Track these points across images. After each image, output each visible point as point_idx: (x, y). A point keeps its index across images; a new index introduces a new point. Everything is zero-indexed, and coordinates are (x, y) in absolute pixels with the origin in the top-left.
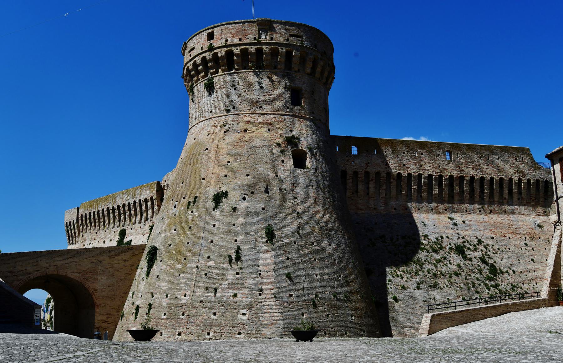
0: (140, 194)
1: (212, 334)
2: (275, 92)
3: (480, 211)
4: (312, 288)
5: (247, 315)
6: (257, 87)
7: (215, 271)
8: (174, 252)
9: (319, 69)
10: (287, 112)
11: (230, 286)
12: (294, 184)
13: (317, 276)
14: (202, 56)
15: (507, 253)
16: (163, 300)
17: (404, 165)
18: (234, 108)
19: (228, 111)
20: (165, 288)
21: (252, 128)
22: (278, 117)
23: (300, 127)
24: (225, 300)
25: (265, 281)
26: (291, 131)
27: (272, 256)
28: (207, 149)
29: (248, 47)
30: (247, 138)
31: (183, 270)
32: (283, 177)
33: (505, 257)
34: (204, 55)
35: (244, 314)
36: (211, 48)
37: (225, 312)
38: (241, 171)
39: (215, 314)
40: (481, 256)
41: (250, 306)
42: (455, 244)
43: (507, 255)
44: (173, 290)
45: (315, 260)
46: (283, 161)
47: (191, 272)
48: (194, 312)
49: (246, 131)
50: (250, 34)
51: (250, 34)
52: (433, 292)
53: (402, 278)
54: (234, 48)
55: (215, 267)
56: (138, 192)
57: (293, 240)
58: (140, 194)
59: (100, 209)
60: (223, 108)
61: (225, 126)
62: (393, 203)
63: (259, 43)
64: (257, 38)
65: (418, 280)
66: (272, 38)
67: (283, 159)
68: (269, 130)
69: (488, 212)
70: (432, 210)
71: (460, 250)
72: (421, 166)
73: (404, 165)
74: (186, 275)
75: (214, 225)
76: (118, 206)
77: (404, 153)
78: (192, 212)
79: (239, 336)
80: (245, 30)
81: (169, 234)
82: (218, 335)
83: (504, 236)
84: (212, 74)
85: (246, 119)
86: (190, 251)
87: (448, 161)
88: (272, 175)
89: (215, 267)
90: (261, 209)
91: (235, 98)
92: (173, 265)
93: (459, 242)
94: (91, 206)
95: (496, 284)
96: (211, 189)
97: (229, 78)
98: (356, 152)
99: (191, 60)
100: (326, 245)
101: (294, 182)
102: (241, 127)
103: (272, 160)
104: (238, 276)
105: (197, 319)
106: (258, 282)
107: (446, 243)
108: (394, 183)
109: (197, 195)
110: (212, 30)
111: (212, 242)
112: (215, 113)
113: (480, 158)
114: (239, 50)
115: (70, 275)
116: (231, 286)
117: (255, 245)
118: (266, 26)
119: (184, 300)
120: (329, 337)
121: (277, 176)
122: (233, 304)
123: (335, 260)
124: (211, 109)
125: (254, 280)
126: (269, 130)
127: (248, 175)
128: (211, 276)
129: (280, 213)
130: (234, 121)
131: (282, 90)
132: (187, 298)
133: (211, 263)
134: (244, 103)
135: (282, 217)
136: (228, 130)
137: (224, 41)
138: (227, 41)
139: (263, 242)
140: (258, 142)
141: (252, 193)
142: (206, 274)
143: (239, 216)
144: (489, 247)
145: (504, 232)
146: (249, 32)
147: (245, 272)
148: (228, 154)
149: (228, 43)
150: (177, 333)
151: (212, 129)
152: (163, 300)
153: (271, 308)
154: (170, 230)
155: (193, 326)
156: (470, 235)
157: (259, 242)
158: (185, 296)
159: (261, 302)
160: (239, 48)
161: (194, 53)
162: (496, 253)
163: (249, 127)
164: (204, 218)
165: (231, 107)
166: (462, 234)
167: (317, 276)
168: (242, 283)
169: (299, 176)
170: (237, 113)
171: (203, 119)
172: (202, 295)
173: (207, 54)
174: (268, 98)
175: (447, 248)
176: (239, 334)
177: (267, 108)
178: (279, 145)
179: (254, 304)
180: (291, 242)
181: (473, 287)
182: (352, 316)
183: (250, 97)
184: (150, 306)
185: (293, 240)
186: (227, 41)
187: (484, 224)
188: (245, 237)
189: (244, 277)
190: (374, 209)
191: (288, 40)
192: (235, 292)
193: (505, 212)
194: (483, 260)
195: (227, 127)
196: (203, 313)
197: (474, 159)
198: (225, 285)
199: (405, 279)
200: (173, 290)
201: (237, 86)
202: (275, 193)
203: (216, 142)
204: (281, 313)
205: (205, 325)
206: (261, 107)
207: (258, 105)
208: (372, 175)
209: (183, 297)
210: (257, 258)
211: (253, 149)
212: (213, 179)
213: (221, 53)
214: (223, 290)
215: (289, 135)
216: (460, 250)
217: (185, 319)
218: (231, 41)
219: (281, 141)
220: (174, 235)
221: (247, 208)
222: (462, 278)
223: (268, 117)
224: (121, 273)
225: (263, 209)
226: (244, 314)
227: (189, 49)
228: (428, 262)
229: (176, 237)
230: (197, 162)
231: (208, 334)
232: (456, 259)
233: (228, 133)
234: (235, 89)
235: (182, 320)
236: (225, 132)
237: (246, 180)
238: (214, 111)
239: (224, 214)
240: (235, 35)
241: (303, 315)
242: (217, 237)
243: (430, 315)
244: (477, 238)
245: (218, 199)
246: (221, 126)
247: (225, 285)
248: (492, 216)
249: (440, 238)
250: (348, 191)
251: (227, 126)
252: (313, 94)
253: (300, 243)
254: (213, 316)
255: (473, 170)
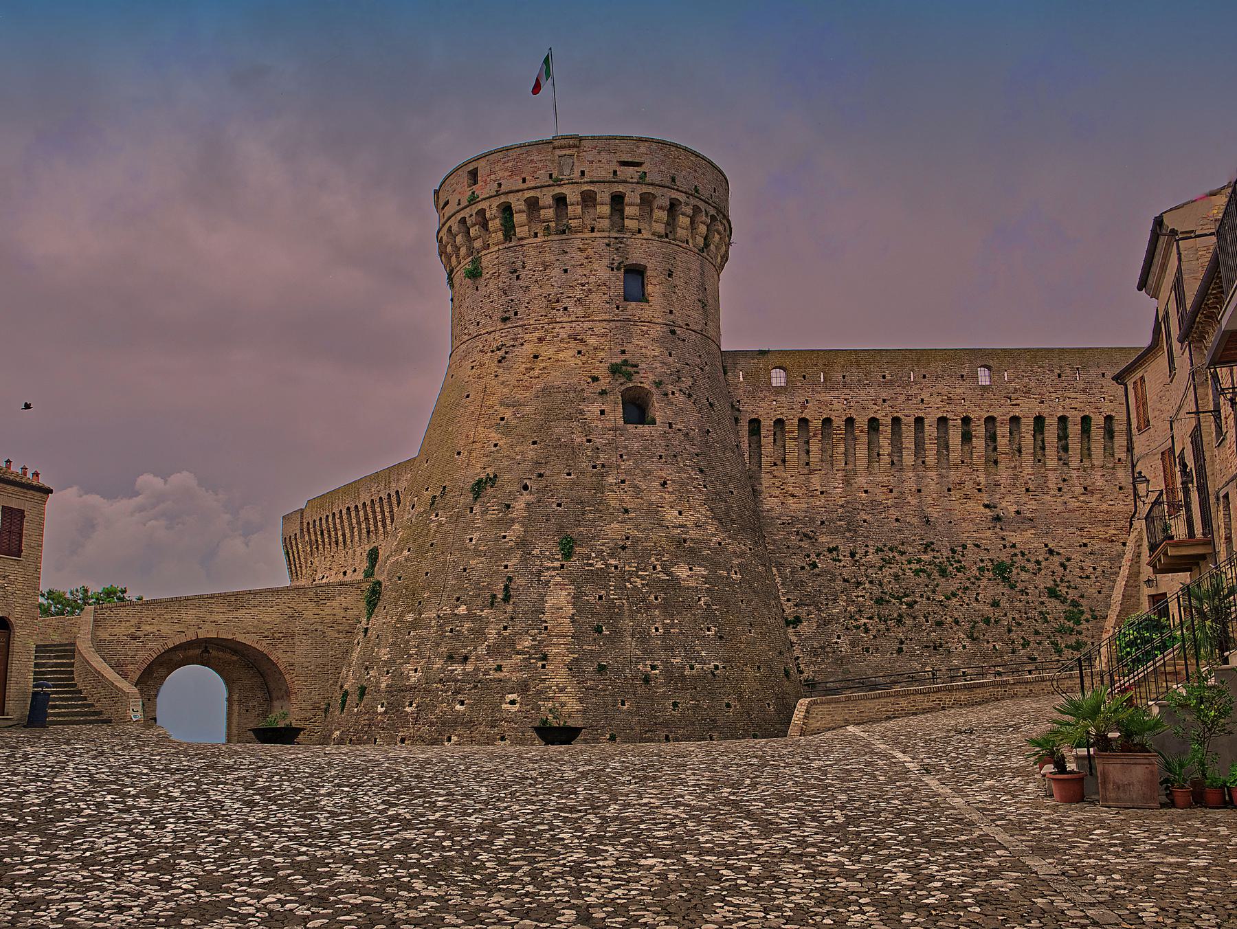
1: (454, 738)
4: (645, 651)
6: (556, 272)
10: (617, 315)
11: (493, 651)
12: (621, 456)
17: (884, 401)
18: (516, 314)
23: (641, 343)
24: (481, 676)
27: (569, 594)
31: (414, 625)
35: (513, 702)
36: (473, 200)
37: (479, 700)
38: (522, 435)
39: (462, 703)
40: (1050, 584)
41: (523, 687)
42: (992, 561)
45: (656, 599)
46: (602, 412)
47: (428, 626)
49: (536, 357)
59: (336, 511)
62: (861, 480)
67: (603, 407)
71: (1002, 571)
72: (922, 400)
75: (471, 540)
81: (400, 558)
85: (537, 334)
87: (984, 388)
93: (1004, 556)
95: (1077, 642)
98: (783, 380)
103: (582, 412)
104: (506, 633)
108: (863, 439)
109: (447, 483)
111: (465, 570)
122: (494, 685)
126: (579, 352)
127: (534, 443)
129: (590, 512)
131: (604, 274)
133: (462, 610)
135: (594, 521)
136: (504, 358)
139: (554, 569)
140: (556, 379)
141: (541, 475)
143: (513, 521)
144: (1073, 566)
146: (539, 165)
148: (502, 404)
153: (562, 690)
157: (548, 569)
159: (545, 680)
161: (449, 210)
162: (1088, 577)
164: (453, 526)
167: (657, 629)
171: (467, 337)
172: (443, 669)
176: (503, 739)
180: (607, 565)
181: (1024, 646)
185: (612, 561)
188: (524, 560)
192: (499, 662)
194: (1052, 593)
198: (482, 649)
202: (582, 473)
204: (581, 701)
205: (443, 724)
206: (566, 309)
208: (816, 424)
210: (542, 598)
211: (547, 391)
212: (474, 454)
214: (478, 658)
216: (1002, 571)
217: (413, 713)
219: (602, 372)
224: (339, 632)
226: (513, 702)
227: (441, 204)
228: (928, 599)
229: (409, 564)
232: (990, 589)
233: (504, 364)
234: (518, 277)
235: (407, 714)
236: (500, 361)
237: (531, 452)
238: (483, 322)
239: (488, 517)
240: (514, 172)
241: (623, 704)
242: (473, 562)
244: (1046, 545)
245: (479, 488)
251: (504, 349)
252: (670, 275)
253: (627, 568)
254: (458, 707)
255: (1042, 402)
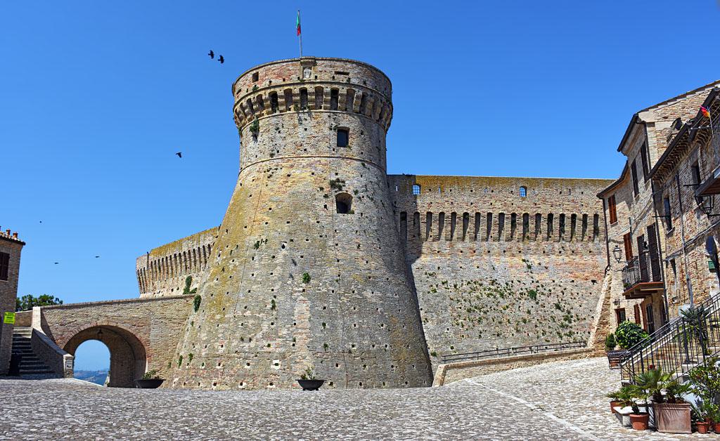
0: (204, 240)
1: (244, 384)
2: (321, 134)
3: (560, 252)
4: (348, 337)
5: (279, 366)
7: (251, 321)
8: (215, 302)
9: (369, 105)
10: (334, 154)
13: (355, 325)
14: (247, 98)
15: (587, 298)
16: (203, 350)
18: (278, 152)
19: (272, 155)
20: (204, 339)
21: (296, 172)
22: (323, 160)
24: (259, 350)
25: (300, 331)
26: (337, 174)
27: (308, 306)
28: (251, 196)
29: (292, 87)
30: (289, 184)
31: (221, 321)
32: (324, 223)
33: (585, 302)
34: (249, 97)
35: (277, 364)
36: (255, 90)
39: (248, 364)
40: (556, 302)
41: (283, 356)
42: (526, 289)
43: (587, 300)
44: (212, 341)
45: (355, 309)
48: (229, 363)
50: (294, 72)
51: (294, 72)
52: (497, 341)
53: (463, 326)
54: (277, 90)
55: (251, 317)
56: (202, 238)
57: (331, 288)
58: (204, 240)
60: (268, 152)
61: (268, 171)
63: (303, 82)
64: (301, 78)
65: (480, 329)
66: (316, 77)
68: (313, 174)
69: (570, 252)
70: (504, 252)
71: (533, 294)
73: (472, 204)
74: (224, 325)
75: (253, 275)
76: (184, 252)
77: (472, 191)
78: (233, 261)
79: (271, 387)
80: (289, 70)
81: (212, 284)
82: (251, 386)
83: (587, 279)
84: (257, 117)
85: (290, 163)
86: (229, 301)
88: (313, 221)
89: (251, 317)
90: (299, 257)
91: (279, 142)
92: (214, 315)
93: (533, 288)
94: (160, 253)
96: (252, 238)
97: (274, 120)
99: (238, 102)
100: (368, 294)
101: (337, 228)
102: (284, 171)
103: (314, 206)
104: (272, 326)
105: (232, 369)
106: (292, 332)
107: (516, 286)
110: (257, 71)
111: (249, 291)
112: (260, 158)
113: (561, 193)
114: (282, 91)
115: (120, 325)
116: (266, 336)
117: (291, 294)
118: (310, 63)
119: (221, 350)
120: (365, 388)
121: (318, 222)
122: (266, 355)
123: (377, 309)
124: (257, 153)
125: (288, 330)
126: (313, 174)
127: (288, 222)
128: (247, 326)
130: (277, 166)
131: (327, 131)
132: (224, 348)
133: (248, 313)
134: (289, 147)
135: (321, 266)
136: (271, 176)
137: (268, 83)
138: (270, 82)
139: (299, 292)
140: (300, 187)
141: (292, 240)
142: (242, 324)
143: (276, 265)
145: (586, 275)
147: (280, 323)
148: (270, 201)
149: (273, 84)
150: (213, 383)
151: (255, 174)
152: (203, 350)
153: (304, 358)
154: (213, 279)
155: (227, 376)
156: (544, 278)
157: (296, 292)
158: (222, 346)
159: (294, 352)
160: (313, 86)
162: (575, 298)
163: (292, 171)
165: (276, 151)
166: (536, 277)
167: (355, 325)
168: (276, 333)
169: (342, 222)
170: (281, 157)
171: (250, 164)
172: (237, 346)
173: (251, 97)
174: (312, 140)
175: (518, 293)
176: (271, 384)
177: (312, 151)
178: (322, 189)
179: (287, 355)
180: (328, 290)
182: (392, 366)
183: (294, 140)
184: (191, 355)
185: (331, 288)
186: (270, 82)
187: (564, 266)
189: (278, 327)
190: (438, 252)
191: (334, 77)
193: (590, 252)
195: (270, 173)
196: (238, 363)
197: (552, 195)
198: (259, 335)
199: (466, 327)
200: (212, 341)
201: (281, 129)
203: (259, 189)
205: (238, 376)
206: (305, 150)
207: (302, 148)
209: (220, 347)
210: (293, 308)
212: (254, 227)
213: (266, 95)
215: (334, 178)
218: (275, 82)
219: (326, 185)
220: (215, 285)
221: (285, 256)
222: (531, 326)
223: (312, 160)
225: (302, 257)
226: (277, 364)
227: (237, 91)
230: (241, 209)
231: (241, 384)
232: (528, 304)
233: (271, 179)
234: (279, 132)
235: (218, 370)
236: (269, 177)
237: (286, 228)
238: (259, 155)
239: (263, 263)
240: (279, 76)
242: (254, 287)
243: (443, 366)
246: (265, 172)
247: (259, 335)
248: (574, 257)
249: (510, 283)
250: (408, 234)
251: (271, 171)
254: (246, 367)
